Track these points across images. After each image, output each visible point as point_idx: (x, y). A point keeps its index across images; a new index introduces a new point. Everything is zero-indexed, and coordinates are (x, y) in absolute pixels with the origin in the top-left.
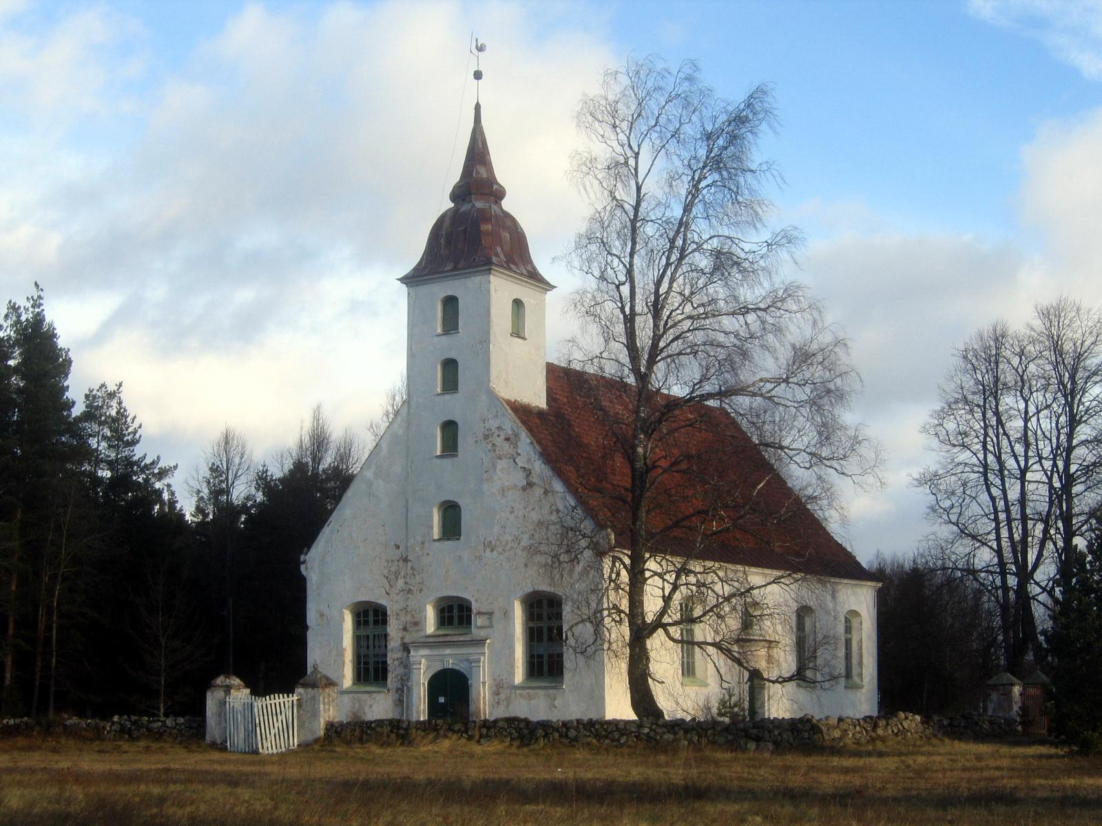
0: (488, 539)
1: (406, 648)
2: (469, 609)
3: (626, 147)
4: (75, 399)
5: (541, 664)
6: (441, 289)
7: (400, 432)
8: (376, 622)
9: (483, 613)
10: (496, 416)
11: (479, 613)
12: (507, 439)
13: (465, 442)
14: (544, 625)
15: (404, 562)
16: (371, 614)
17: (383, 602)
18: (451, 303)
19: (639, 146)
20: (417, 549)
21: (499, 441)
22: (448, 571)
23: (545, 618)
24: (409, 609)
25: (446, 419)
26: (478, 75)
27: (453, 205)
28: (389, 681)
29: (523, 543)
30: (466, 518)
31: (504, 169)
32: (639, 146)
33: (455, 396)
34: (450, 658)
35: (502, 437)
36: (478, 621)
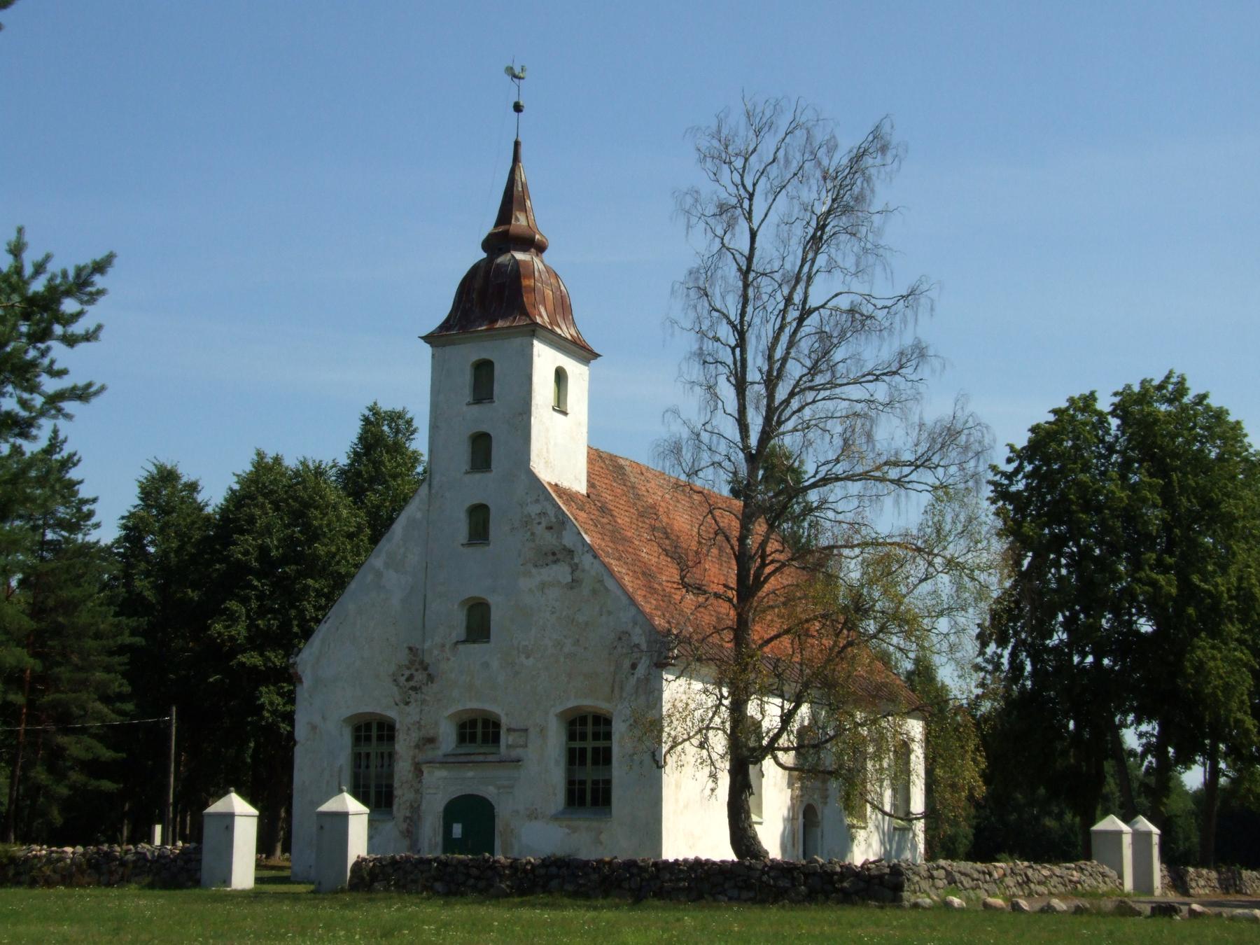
0: (524, 643)
1: (418, 770)
2: (497, 725)
3: (740, 187)
4: (370, 404)
5: (583, 793)
6: (468, 353)
7: (419, 515)
8: (380, 738)
9: (514, 730)
10: (537, 501)
11: (509, 730)
12: (549, 528)
13: (497, 529)
14: (589, 744)
15: (417, 672)
16: (480, 725)
17: (392, 714)
18: (483, 371)
19: (754, 185)
20: (436, 652)
21: (539, 530)
22: (472, 679)
23: (590, 736)
24: (423, 723)
25: (476, 502)
26: (518, 108)
27: (484, 255)
28: (395, 807)
29: (566, 650)
30: (495, 617)
31: (540, 216)
32: (754, 185)
33: (488, 475)
34: (472, 781)
35: (544, 525)
36: (505, 739)
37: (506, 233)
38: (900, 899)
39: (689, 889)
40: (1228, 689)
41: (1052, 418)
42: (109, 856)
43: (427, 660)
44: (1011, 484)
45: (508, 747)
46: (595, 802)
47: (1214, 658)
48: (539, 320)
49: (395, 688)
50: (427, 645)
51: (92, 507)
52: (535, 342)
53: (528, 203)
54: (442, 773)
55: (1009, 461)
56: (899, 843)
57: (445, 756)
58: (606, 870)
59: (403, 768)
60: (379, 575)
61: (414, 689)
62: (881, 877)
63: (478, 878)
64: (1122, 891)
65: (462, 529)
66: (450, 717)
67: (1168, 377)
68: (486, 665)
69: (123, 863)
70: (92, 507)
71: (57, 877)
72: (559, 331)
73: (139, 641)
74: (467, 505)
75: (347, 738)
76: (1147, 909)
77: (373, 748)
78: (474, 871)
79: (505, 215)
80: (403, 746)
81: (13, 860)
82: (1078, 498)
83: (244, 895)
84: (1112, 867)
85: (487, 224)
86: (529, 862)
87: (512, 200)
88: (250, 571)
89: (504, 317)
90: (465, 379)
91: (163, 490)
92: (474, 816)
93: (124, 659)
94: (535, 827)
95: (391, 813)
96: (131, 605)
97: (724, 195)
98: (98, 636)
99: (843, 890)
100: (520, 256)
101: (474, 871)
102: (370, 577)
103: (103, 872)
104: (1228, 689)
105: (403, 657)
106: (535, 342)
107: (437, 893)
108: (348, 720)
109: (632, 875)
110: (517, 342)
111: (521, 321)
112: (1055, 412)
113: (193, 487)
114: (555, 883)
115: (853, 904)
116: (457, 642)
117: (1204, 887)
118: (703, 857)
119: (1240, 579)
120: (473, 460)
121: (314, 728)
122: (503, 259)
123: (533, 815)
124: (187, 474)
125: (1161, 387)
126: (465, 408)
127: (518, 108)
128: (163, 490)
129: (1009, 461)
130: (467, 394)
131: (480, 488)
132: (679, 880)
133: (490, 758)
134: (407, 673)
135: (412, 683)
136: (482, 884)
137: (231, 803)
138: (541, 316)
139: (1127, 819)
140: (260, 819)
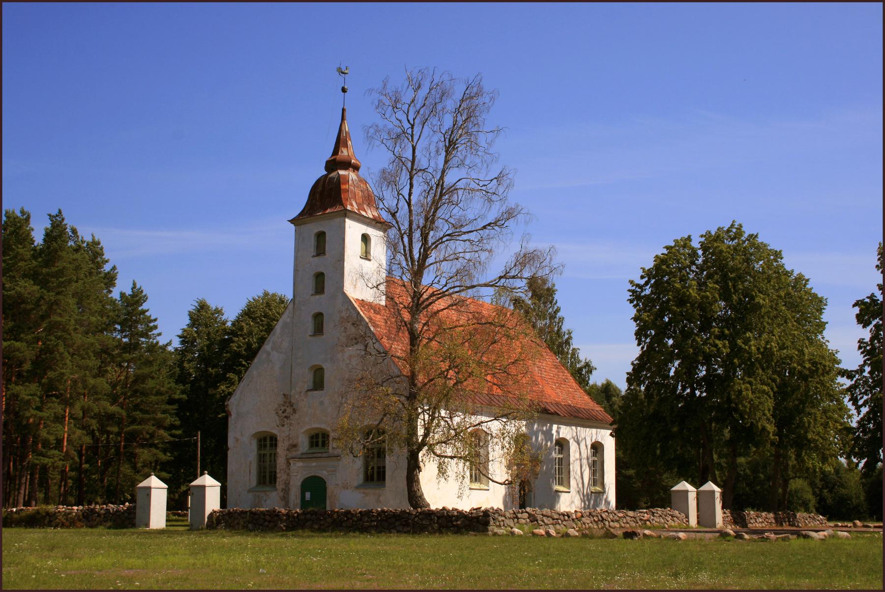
1: (288, 464)
6: (313, 228)
7: (288, 320)
8: (271, 445)
15: (288, 408)
17: (275, 432)
18: (321, 237)
22: (318, 411)
26: (344, 90)
30: (327, 375)
36: (332, 444)
37: (335, 159)
38: (487, 531)
39: (376, 526)
40: (754, 408)
41: (665, 251)
42: (93, 511)
43: (293, 401)
44: (642, 291)
45: (333, 448)
46: (379, 480)
47: (747, 389)
48: (349, 208)
49: (277, 418)
50: (293, 392)
51: (155, 323)
52: (347, 220)
53: (349, 143)
54: (300, 464)
55: (642, 277)
56: (595, 501)
57: (302, 454)
58: (335, 516)
59: (281, 462)
60: (269, 354)
61: (286, 417)
62: (477, 518)
63: (270, 522)
64: (688, 526)
65: (309, 325)
66: (304, 433)
67: (732, 226)
68: (322, 403)
69: (99, 515)
70: (155, 323)
71: (67, 523)
72: (364, 213)
73: (184, 396)
74: (313, 313)
75: (254, 446)
76: (620, 533)
77: (267, 451)
78: (268, 518)
79: (336, 152)
80: (281, 450)
81: (48, 514)
82: (674, 297)
83: (160, 532)
84: (680, 512)
85: (328, 155)
86: (296, 512)
87: (340, 142)
88: (242, 356)
89: (331, 207)
90: (312, 242)
91: (202, 316)
92: (315, 487)
93: (175, 407)
94: (347, 494)
95: (275, 487)
96: (182, 378)
97: (391, 126)
98: (159, 393)
99: (457, 526)
100: (342, 172)
101: (268, 518)
102: (264, 356)
103: (89, 520)
104: (754, 408)
105: (281, 399)
106: (347, 220)
107: (251, 531)
108: (254, 435)
109: (348, 519)
110: (337, 220)
111: (338, 208)
112: (667, 248)
113: (218, 311)
114: (308, 524)
115: (462, 534)
116: (308, 390)
117: (762, 522)
118: (450, 507)
119: (767, 343)
120: (316, 288)
121: (237, 440)
122: (333, 175)
123: (346, 487)
124: (213, 304)
125: (728, 231)
126: (312, 259)
127: (344, 90)
128: (202, 316)
129: (642, 277)
130: (312, 250)
131: (319, 303)
132: (372, 521)
133: (324, 455)
134: (283, 408)
135: (285, 414)
136: (272, 524)
137: (150, 482)
138: (352, 205)
139: (697, 484)
140: (170, 491)
